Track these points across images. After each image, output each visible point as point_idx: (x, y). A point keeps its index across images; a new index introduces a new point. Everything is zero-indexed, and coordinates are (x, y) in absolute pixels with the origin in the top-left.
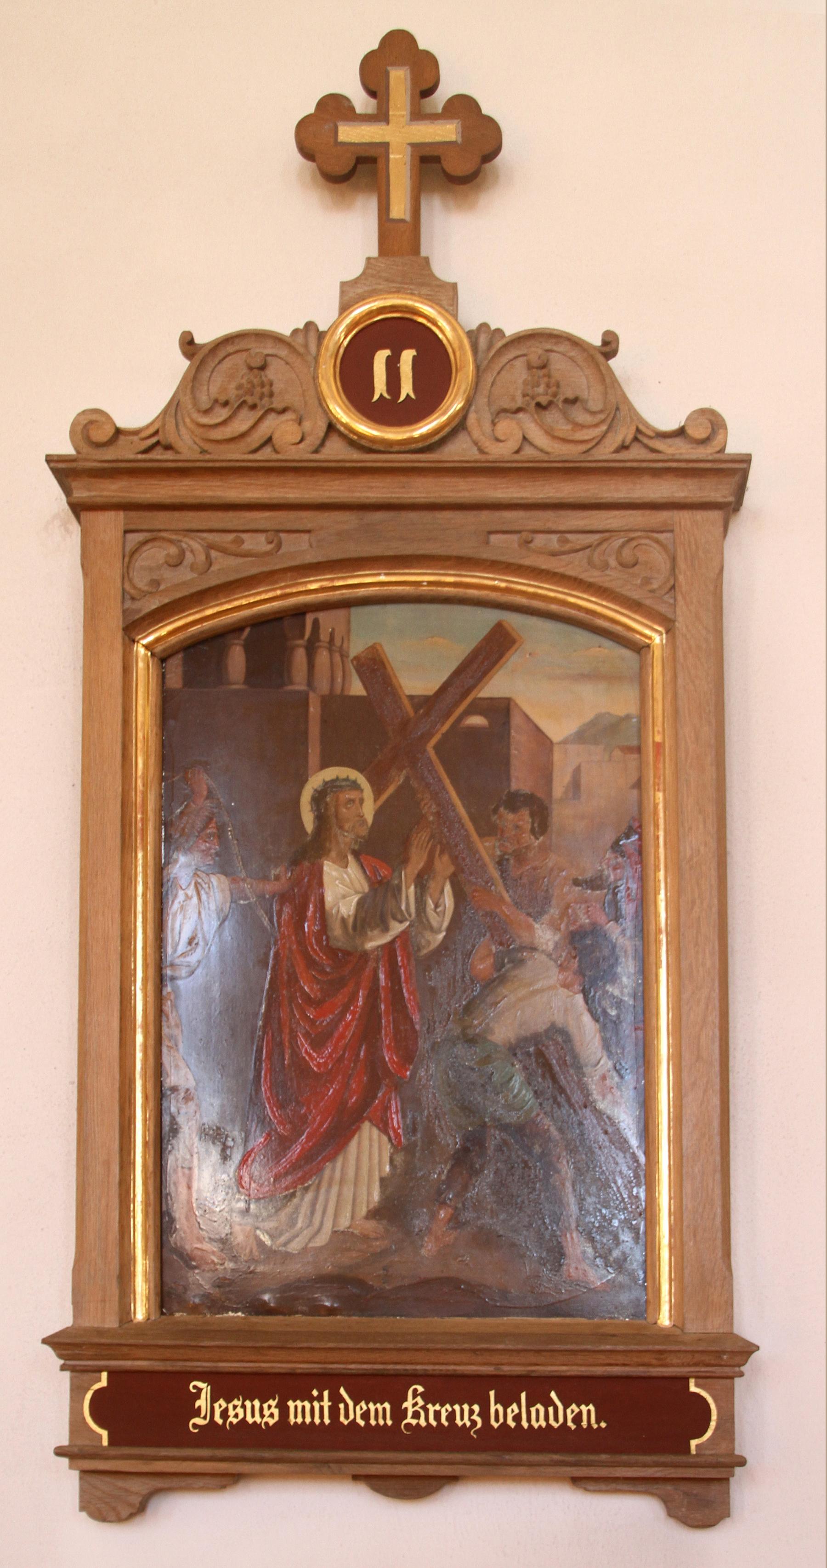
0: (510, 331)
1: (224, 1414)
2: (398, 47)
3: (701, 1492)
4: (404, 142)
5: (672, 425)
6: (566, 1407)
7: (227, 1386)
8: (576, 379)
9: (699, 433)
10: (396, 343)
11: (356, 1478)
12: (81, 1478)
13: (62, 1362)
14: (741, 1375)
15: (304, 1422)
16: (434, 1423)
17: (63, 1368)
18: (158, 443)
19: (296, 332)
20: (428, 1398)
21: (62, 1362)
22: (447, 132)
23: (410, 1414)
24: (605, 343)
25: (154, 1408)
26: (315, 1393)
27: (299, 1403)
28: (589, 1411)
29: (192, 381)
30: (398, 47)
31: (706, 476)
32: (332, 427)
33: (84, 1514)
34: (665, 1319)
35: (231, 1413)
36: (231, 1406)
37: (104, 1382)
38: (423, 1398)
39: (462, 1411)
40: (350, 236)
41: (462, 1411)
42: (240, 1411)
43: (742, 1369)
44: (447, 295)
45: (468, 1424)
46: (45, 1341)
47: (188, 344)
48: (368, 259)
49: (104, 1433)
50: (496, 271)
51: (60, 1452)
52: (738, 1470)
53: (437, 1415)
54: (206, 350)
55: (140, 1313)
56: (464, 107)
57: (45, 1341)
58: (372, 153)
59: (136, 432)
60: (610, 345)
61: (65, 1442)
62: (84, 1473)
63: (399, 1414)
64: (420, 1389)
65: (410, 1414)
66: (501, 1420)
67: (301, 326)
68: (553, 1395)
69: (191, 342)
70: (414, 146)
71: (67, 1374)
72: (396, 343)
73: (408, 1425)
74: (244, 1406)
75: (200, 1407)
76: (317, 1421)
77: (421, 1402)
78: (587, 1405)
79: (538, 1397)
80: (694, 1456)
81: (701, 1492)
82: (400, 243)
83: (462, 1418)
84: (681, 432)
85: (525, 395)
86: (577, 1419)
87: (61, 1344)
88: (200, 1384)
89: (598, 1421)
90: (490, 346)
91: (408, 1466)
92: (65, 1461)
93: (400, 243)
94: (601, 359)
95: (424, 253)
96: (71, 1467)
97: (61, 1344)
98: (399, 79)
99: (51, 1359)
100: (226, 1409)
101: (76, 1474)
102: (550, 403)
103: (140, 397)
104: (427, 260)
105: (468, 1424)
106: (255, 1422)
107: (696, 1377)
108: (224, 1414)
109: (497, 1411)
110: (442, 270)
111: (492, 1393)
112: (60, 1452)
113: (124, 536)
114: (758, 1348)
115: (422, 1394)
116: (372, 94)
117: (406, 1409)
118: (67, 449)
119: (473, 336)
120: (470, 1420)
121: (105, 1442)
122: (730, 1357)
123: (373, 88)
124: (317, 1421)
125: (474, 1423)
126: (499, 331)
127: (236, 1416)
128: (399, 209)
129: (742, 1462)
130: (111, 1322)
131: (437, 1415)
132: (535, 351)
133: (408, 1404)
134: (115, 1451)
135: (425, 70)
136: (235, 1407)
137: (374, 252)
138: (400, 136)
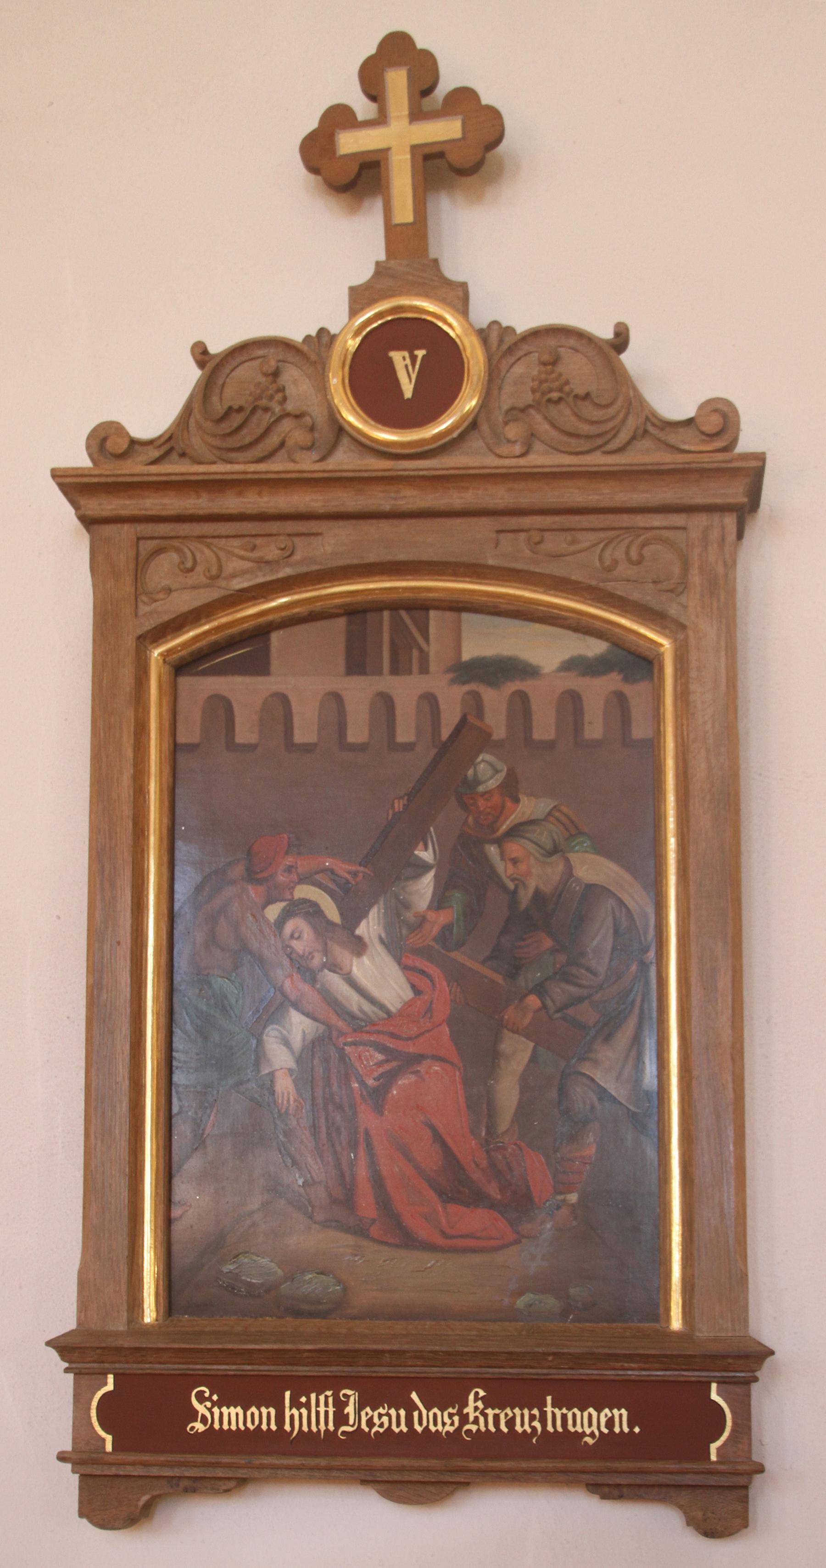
0: (522, 325)
1: (370, 1423)
2: (397, 48)
3: (721, 1500)
4: (412, 142)
5: (687, 411)
6: (428, 1410)
7: (231, 1392)
8: (577, 370)
9: (712, 423)
10: (404, 351)
11: (364, 1482)
12: (81, 1481)
13: (66, 1365)
14: (756, 1380)
15: (230, 1429)
16: (492, 1428)
17: (67, 1370)
18: (172, 449)
19: (308, 338)
20: (488, 1402)
21: (66, 1365)
22: (446, 130)
23: (471, 1418)
24: (617, 334)
25: (157, 1412)
26: (303, 1399)
27: (232, 1409)
28: (621, 1416)
29: (207, 388)
30: (397, 48)
31: (711, 479)
32: (340, 430)
33: (85, 1521)
34: (676, 1323)
35: (376, 1420)
36: (376, 1414)
37: (110, 1387)
38: (483, 1403)
39: (522, 1416)
40: (356, 243)
41: (522, 1416)
42: (385, 1419)
43: (758, 1374)
44: (459, 296)
45: (529, 1430)
46: (48, 1344)
47: (201, 354)
48: (378, 264)
49: (109, 1438)
50: (510, 268)
51: (62, 1457)
52: (758, 1478)
53: (496, 1418)
54: (218, 360)
55: (149, 1315)
56: (464, 99)
57: (48, 1344)
58: (373, 158)
59: (150, 442)
60: (621, 340)
61: (68, 1447)
62: (84, 1477)
63: (341, 1419)
64: (482, 1393)
65: (471, 1418)
66: (425, 1423)
67: (313, 333)
68: (414, 1396)
69: (205, 352)
70: (414, 148)
71: (71, 1376)
72: (404, 351)
73: (469, 1432)
74: (389, 1415)
75: (348, 1414)
76: (305, 1428)
77: (480, 1404)
78: (235, 1407)
79: (447, 1394)
80: (714, 1463)
81: (721, 1500)
82: (411, 255)
83: (522, 1425)
84: (690, 422)
85: (534, 391)
86: (610, 1423)
87: (64, 1347)
88: (349, 1392)
89: (631, 1426)
90: (501, 341)
91: (421, 1472)
92: (68, 1466)
93: (411, 255)
94: (612, 353)
95: (432, 256)
96: (74, 1471)
97: (64, 1347)
98: (397, 81)
99: (55, 1362)
100: (372, 1416)
101: (77, 1476)
102: (560, 399)
103: (151, 414)
104: (436, 262)
105: (529, 1430)
106: (437, 1431)
107: (718, 1383)
108: (370, 1423)
109: (292, 1417)
110: (452, 271)
111: (549, 1399)
112: (62, 1457)
113: (138, 543)
114: (772, 1353)
115: (482, 1398)
116: (373, 98)
117: (468, 1414)
118: (82, 460)
119: (483, 334)
120: (531, 1426)
121: (109, 1447)
122: (745, 1362)
123: (374, 93)
124: (305, 1428)
125: (534, 1429)
126: (510, 330)
127: (381, 1425)
128: (404, 214)
129: (760, 1469)
130: (120, 1325)
131: (496, 1418)
132: (273, 356)
133: (469, 1410)
134: (121, 1457)
135: (423, 68)
136: (380, 1416)
137: (382, 257)
138: (398, 137)
